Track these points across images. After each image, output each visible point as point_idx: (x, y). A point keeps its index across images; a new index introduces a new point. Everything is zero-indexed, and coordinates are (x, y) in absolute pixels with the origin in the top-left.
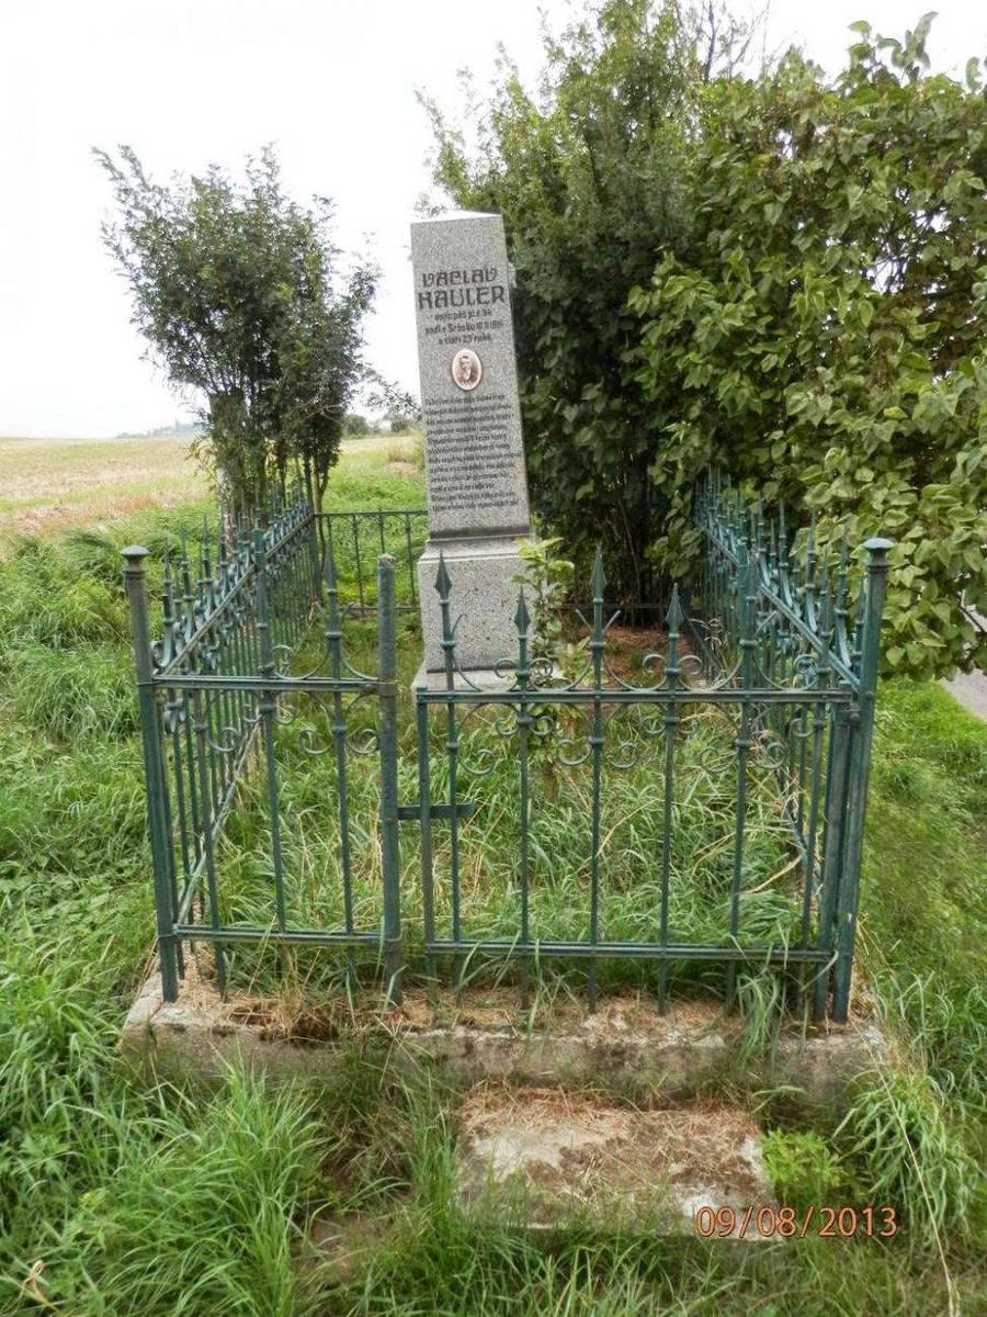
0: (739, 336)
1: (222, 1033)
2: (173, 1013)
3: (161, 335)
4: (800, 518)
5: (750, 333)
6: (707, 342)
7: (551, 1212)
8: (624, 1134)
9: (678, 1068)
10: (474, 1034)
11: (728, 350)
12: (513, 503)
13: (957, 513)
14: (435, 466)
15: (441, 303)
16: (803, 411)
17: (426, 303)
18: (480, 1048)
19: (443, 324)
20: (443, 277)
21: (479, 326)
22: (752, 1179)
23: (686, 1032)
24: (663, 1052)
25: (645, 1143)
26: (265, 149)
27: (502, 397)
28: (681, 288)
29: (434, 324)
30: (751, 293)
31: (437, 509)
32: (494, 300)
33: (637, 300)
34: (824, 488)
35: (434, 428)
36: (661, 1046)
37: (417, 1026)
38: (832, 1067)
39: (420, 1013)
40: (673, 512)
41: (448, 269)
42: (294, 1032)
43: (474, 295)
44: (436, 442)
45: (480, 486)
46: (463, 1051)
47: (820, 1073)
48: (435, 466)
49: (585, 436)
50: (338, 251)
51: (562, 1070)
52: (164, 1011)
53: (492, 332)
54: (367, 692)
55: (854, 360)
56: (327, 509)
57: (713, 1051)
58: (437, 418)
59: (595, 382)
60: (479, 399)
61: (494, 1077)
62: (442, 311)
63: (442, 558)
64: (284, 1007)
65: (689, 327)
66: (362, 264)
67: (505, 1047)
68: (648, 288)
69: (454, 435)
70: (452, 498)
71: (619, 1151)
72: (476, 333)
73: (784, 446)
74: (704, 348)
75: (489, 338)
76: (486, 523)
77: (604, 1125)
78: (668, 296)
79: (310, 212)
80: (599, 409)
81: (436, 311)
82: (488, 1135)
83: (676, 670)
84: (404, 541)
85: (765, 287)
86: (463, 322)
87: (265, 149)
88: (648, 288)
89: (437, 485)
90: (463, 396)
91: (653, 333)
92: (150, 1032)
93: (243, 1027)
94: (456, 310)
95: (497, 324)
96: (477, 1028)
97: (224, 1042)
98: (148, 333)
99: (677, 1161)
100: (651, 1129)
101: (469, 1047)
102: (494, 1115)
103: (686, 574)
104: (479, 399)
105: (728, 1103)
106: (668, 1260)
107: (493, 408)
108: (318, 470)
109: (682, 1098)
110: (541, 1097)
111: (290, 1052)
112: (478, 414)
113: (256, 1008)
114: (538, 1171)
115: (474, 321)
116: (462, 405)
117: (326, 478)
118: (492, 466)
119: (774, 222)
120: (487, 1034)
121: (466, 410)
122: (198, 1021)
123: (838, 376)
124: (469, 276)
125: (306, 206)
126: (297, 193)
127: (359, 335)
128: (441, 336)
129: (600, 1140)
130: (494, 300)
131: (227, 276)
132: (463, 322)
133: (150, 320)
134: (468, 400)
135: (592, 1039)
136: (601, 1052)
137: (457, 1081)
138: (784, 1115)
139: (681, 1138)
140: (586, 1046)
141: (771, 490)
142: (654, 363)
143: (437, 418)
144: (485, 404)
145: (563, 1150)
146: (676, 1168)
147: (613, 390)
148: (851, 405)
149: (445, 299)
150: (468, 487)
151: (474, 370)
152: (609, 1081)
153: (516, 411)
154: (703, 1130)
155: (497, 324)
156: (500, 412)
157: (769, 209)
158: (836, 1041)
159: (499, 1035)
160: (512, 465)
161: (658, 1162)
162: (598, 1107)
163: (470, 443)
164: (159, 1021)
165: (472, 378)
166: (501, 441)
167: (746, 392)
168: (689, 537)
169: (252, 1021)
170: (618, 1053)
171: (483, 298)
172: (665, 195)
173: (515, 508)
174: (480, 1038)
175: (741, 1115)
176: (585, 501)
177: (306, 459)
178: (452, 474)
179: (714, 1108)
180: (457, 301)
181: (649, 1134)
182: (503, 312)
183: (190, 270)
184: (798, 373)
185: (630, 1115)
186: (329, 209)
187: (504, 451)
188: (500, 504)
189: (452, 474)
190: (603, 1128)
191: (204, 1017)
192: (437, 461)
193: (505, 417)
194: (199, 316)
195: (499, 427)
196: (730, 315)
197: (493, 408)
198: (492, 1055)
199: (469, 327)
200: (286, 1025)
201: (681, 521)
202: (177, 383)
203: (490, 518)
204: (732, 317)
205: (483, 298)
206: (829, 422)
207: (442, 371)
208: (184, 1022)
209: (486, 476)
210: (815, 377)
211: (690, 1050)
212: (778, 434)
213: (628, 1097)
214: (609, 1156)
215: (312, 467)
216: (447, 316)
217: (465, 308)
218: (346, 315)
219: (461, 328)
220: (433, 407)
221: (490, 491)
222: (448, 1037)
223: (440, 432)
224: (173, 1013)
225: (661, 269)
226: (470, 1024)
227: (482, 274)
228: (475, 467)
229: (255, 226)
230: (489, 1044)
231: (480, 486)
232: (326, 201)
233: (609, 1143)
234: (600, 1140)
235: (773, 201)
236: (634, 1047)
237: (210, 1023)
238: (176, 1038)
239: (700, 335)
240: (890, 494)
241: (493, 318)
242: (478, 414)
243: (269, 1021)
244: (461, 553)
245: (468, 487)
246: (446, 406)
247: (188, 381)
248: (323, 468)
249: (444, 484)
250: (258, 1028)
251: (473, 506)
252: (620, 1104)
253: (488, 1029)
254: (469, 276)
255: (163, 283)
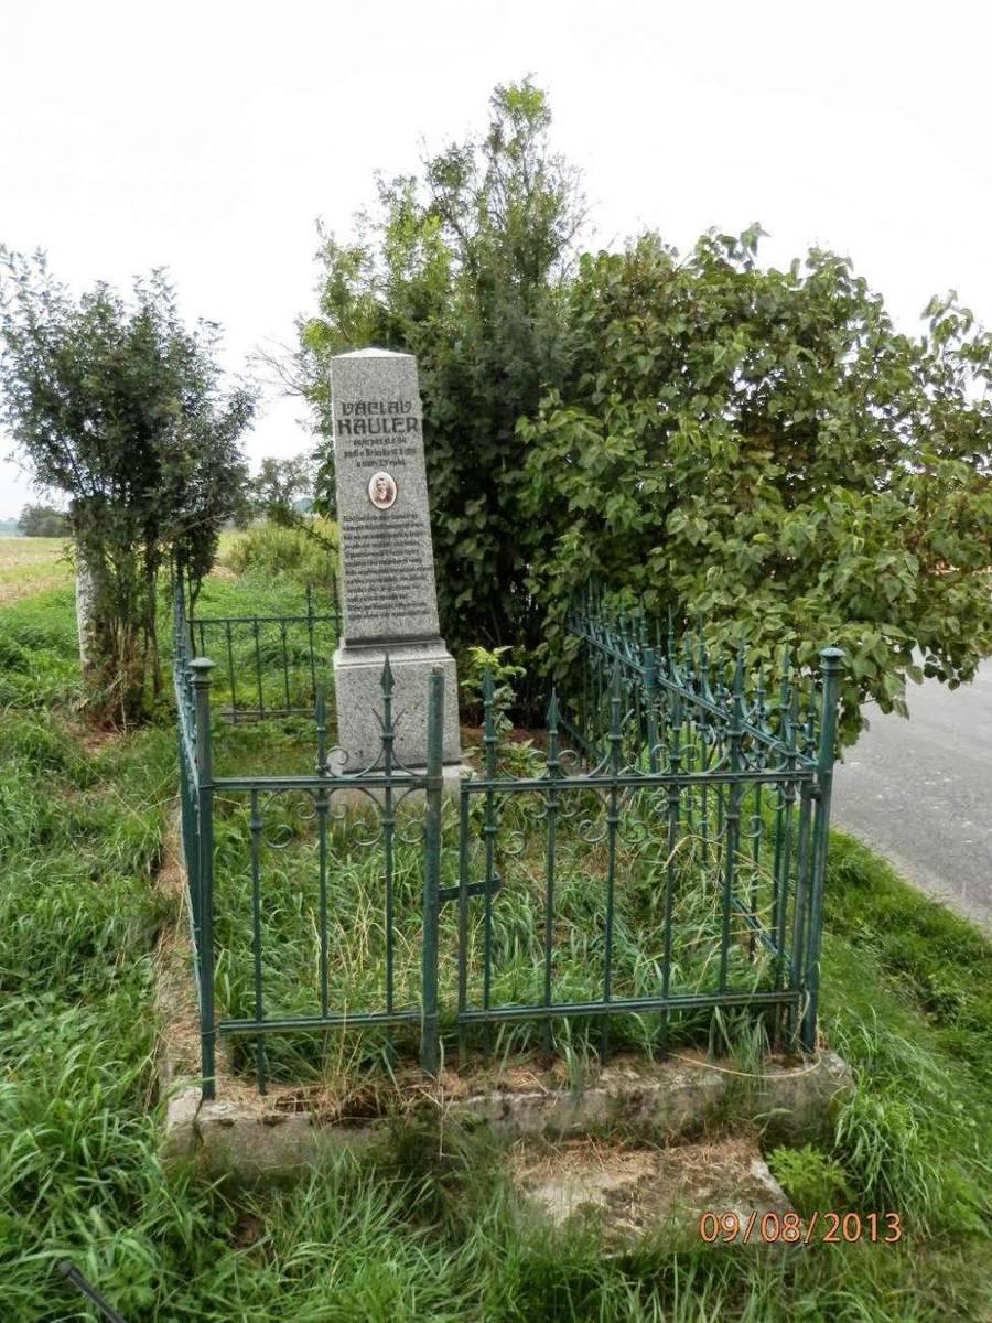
0: (620, 467)
1: (271, 1123)
2: (217, 1110)
3: (36, 441)
4: (684, 624)
5: (629, 464)
6: (593, 467)
7: (618, 1242)
8: (651, 1171)
9: (686, 1106)
10: (509, 1096)
11: (612, 477)
12: (425, 613)
13: (826, 620)
14: (352, 578)
15: (360, 430)
16: (682, 532)
17: (345, 430)
18: (516, 1109)
19: (361, 449)
20: (361, 407)
21: (394, 452)
22: (769, 1192)
23: (690, 1079)
24: (674, 1094)
25: (671, 1176)
26: (155, 272)
27: (415, 516)
28: (573, 423)
29: (353, 448)
30: (628, 431)
31: (352, 618)
32: (409, 429)
33: (524, 428)
34: (706, 598)
35: (352, 542)
36: (672, 1088)
37: (451, 1093)
38: (810, 1090)
39: (458, 1085)
40: (547, 620)
41: (366, 400)
42: (345, 1112)
43: (390, 425)
44: (353, 555)
45: (394, 597)
46: (501, 1113)
47: (800, 1097)
48: (352, 578)
49: (469, 548)
50: (218, 371)
51: (589, 1122)
52: (206, 1108)
53: (407, 458)
54: (414, 784)
55: (721, 491)
56: (198, 617)
57: (716, 1088)
58: (354, 533)
59: (477, 498)
60: (394, 517)
61: (529, 1134)
62: (359, 438)
63: (387, 663)
64: (334, 1089)
65: (575, 454)
66: (242, 386)
67: (539, 1105)
68: (532, 414)
69: (371, 550)
70: (367, 608)
71: (652, 1185)
72: (391, 458)
73: (663, 560)
74: (590, 473)
75: (402, 463)
76: (399, 631)
77: (632, 1165)
78: (553, 427)
79: (196, 334)
80: (481, 524)
81: (354, 437)
82: (535, 1187)
83: (556, 762)
84: (252, 643)
85: (642, 424)
86: (379, 447)
87: (155, 272)
88: (532, 414)
89: (353, 595)
90: (378, 514)
91: (536, 459)
92: (197, 1130)
93: (292, 1116)
94: (373, 437)
95: (411, 451)
96: (511, 1091)
97: (275, 1131)
98: (17, 435)
99: (704, 1186)
100: (672, 1164)
101: (506, 1109)
102: (533, 1170)
103: (565, 677)
104: (394, 517)
105: (731, 1133)
106: (716, 1269)
107: (407, 525)
108: (192, 577)
109: (693, 1134)
110: (573, 1148)
111: (340, 1134)
112: (393, 531)
113: (300, 1096)
114: (587, 1210)
115: (390, 447)
116: (378, 523)
117: (199, 584)
118: (404, 579)
119: (646, 372)
120: (522, 1096)
121: (382, 526)
122: (245, 1114)
123: (708, 504)
124: (386, 407)
125: (189, 327)
126: (187, 315)
127: (239, 448)
128: (359, 459)
129: (633, 1179)
130: (409, 429)
131: (111, 385)
132: (379, 447)
133: (17, 423)
134: (384, 518)
135: (613, 1089)
136: (622, 1100)
137: (493, 1138)
138: (775, 1136)
139: (699, 1168)
140: (609, 1096)
141: (651, 597)
142: (537, 485)
143: (354, 533)
144: (400, 522)
145: (605, 1191)
146: (703, 1192)
147: (491, 507)
148: (720, 529)
149: (362, 426)
150: (383, 598)
151: (389, 491)
152: (629, 1128)
153: (427, 528)
154: (716, 1159)
155: (411, 451)
156: (413, 530)
157: (641, 360)
158: (809, 1070)
159: (532, 1095)
160: (423, 578)
161: (686, 1189)
162: (622, 1151)
163: (385, 558)
164: (205, 1119)
165: (388, 498)
166: (414, 556)
167: (630, 512)
168: (571, 643)
169: (299, 1108)
170: (637, 1099)
171: (399, 428)
172: (553, 340)
173: (426, 617)
174: (516, 1099)
175: (741, 1143)
176: (465, 607)
177: (179, 565)
178: (368, 585)
179: (723, 1137)
180: (374, 429)
181: (672, 1169)
182: (416, 440)
183: (69, 377)
184: (673, 500)
185: (651, 1154)
186: (217, 333)
187: (416, 565)
188: (412, 614)
189: (368, 585)
190: (632, 1169)
191: (251, 1110)
192: (353, 573)
193: (417, 534)
194: (74, 427)
195: (411, 543)
196: (614, 446)
197: (407, 525)
198: (527, 1115)
199: (385, 453)
200: (336, 1108)
201: (555, 629)
202: (43, 485)
203: (402, 626)
204: (617, 447)
205: (399, 428)
206: (704, 541)
207: (359, 491)
208: (233, 1117)
209: (399, 588)
210: (692, 503)
211: (696, 1089)
212: (658, 550)
213: (646, 1140)
214: (645, 1191)
215: (186, 574)
216: (365, 442)
217: (382, 435)
218: (223, 428)
219: (377, 453)
220: (351, 524)
221: (404, 601)
222: (487, 1102)
223: (357, 546)
224: (217, 1110)
225: (544, 403)
226: (504, 1088)
227: (398, 406)
228: (390, 579)
229: (143, 337)
230: (524, 1104)
231: (394, 597)
232: (215, 325)
233: (642, 1179)
234: (633, 1179)
235: (645, 353)
236: (649, 1093)
237: (260, 1115)
238: (223, 1133)
239: (588, 460)
240: (766, 605)
241: (406, 446)
242: (393, 531)
243: (317, 1106)
244: (406, 657)
245: (383, 598)
246: (363, 523)
247: (57, 485)
248: (197, 575)
249: (360, 595)
250: (306, 1115)
251: (387, 615)
252: (639, 1146)
253: (521, 1090)
254: (386, 407)
255: (36, 386)
